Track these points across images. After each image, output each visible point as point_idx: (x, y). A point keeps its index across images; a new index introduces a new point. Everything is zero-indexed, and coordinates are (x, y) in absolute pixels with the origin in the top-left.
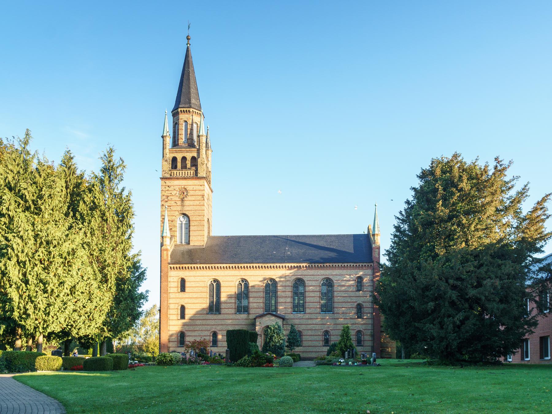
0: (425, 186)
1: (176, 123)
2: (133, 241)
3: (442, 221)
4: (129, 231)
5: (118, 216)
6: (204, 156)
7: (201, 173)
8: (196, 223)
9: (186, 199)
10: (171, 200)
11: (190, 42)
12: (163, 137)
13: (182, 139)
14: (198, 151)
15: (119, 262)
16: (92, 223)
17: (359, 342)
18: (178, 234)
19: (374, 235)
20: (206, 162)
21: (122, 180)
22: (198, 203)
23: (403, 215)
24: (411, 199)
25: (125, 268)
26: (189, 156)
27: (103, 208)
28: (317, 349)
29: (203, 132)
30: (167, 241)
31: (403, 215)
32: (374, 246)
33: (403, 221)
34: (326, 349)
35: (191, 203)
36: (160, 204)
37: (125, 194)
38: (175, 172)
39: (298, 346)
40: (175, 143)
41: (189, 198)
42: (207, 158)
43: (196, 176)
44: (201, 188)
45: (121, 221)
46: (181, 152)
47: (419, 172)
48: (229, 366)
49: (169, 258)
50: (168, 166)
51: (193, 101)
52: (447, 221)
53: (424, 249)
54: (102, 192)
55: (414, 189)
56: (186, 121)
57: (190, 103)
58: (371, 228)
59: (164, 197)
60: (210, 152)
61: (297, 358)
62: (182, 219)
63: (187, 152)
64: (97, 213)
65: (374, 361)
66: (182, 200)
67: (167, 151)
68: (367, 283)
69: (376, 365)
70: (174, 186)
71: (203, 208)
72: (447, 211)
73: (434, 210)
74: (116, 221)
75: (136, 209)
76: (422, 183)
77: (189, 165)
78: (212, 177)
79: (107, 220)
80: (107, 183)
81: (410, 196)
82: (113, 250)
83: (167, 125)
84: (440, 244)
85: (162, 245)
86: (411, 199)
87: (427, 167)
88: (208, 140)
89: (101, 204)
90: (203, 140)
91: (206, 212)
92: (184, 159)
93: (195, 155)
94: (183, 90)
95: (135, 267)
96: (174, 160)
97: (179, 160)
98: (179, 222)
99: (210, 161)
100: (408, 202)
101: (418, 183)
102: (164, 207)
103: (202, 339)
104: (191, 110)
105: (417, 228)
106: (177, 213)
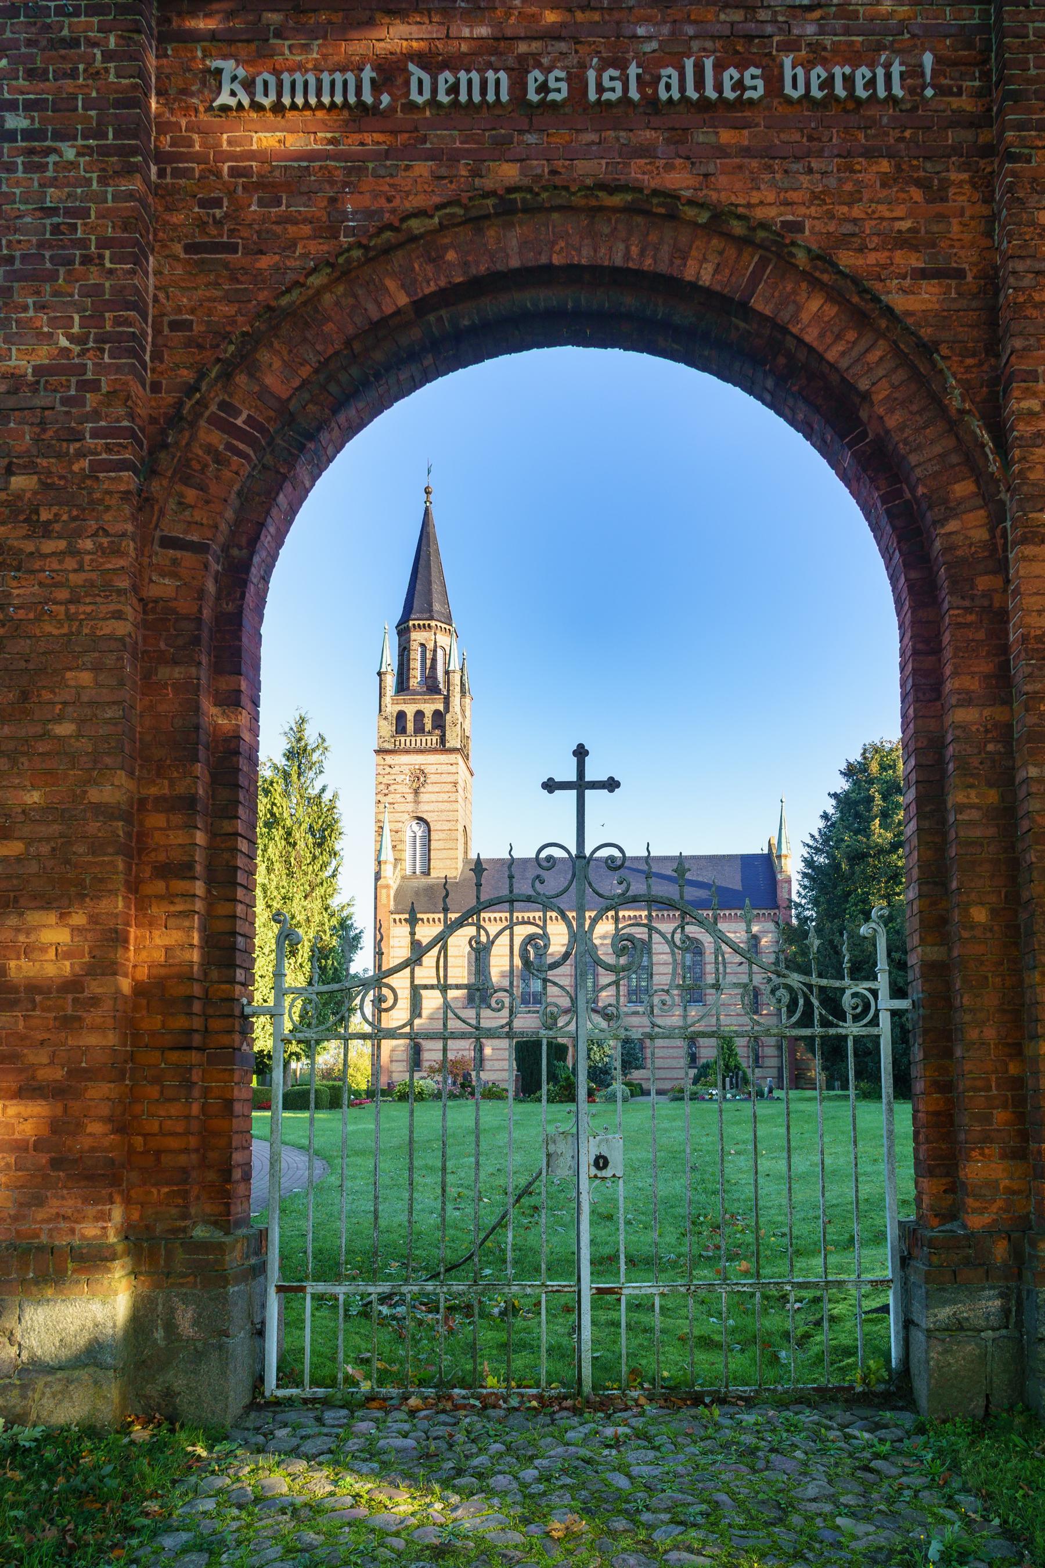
0: (853, 791)
1: (405, 648)
2: (341, 881)
3: (881, 851)
4: (334, 863)
5: (314, 836)
6: (458, 709)
7: (453, 742)
8: (442, 835)
9: (422, 790)
10: (395, 792)
11: (432, 497)
12: (379, 674)
13: (416, 678)
14: (447, 701)
15: (317, 918)
16: (270, 850)
17: (757, 1060)
18: (407, 855)
19: (779, 857)
20: (461, 719)
21: (321, 772)
22: (445, 797)
23: (815, 840)
24: (831, 811)
25: (327, 928)
26: (428, 709)
27: (289, 823)
28: (675, 1074)
29: (455, 665)
30: (387, 871)
31: (815, 840)
32: (779, 877)
33: (818, 851)
34: (693, 1072)
35: (433, 797)
36: (373, 799)
37: (327, 796)
38: (403, 739)
39: (637, 1068)
40: (402, 686)
41: (429, 788)
42: (463, 711)
43: (442, 747)
44: (453, 769)
45: (320, 845)
46: (414, 701)
47: (843, 766)
48: (521, 1101)
49: (392, 903)
50: (388, 728)
51: (437, 607)
52: (890, 852)
53: (852, 899)
54: (286, 794)
55: (835, 796)
56: (422, 645)
57: (431, 611)
58: (775, 841)
59: (382, 787)
60: (467, 700)
61: (638, 1091)
62: (416, 828)
63: (425, 701)
64: (278, 833)
65: (770, 1091)
66: (416, 792)
67: (387, 700)
68: (767, 947)
69: (772, 1098)
70: (400, 765)
71: (455, 806)
72: (890, 835)
73: (866, 832)
74: (311, 845)
75: (344, 825)
76: (846, 788)
77: (428, 727)
78: (473, 749)
79: (295, 844)
80: (294, 777)
81: (829, 806)
82: (306, 897)
83: (387, 653)
84: (879, 890)
85: (378, 877)
86: (831, 811)
87: (856, 757)
88: (465, 678)
89: (286, 815)
90: (456, 679)
91: (460, 815)
92: (419, 714)
93: (441, 707)
94: (418, 587)
95: (344, 925)
96: (401, 716)
97: (410, 717)
98: (410, 834)
99: (466, 717)
100: (825, 816)
101: (842, 785)
102: (381, 806)
103: (459, 1056)
104: (433, 623)
105: (840, 864)
106: (406, 816)
